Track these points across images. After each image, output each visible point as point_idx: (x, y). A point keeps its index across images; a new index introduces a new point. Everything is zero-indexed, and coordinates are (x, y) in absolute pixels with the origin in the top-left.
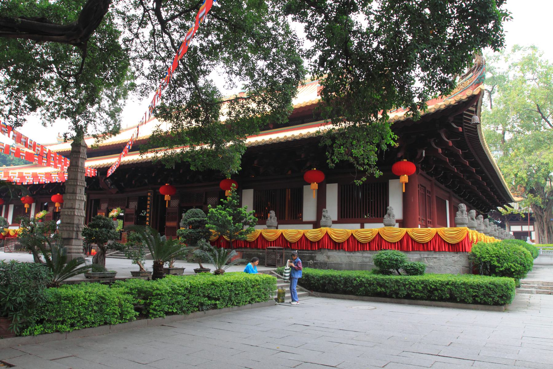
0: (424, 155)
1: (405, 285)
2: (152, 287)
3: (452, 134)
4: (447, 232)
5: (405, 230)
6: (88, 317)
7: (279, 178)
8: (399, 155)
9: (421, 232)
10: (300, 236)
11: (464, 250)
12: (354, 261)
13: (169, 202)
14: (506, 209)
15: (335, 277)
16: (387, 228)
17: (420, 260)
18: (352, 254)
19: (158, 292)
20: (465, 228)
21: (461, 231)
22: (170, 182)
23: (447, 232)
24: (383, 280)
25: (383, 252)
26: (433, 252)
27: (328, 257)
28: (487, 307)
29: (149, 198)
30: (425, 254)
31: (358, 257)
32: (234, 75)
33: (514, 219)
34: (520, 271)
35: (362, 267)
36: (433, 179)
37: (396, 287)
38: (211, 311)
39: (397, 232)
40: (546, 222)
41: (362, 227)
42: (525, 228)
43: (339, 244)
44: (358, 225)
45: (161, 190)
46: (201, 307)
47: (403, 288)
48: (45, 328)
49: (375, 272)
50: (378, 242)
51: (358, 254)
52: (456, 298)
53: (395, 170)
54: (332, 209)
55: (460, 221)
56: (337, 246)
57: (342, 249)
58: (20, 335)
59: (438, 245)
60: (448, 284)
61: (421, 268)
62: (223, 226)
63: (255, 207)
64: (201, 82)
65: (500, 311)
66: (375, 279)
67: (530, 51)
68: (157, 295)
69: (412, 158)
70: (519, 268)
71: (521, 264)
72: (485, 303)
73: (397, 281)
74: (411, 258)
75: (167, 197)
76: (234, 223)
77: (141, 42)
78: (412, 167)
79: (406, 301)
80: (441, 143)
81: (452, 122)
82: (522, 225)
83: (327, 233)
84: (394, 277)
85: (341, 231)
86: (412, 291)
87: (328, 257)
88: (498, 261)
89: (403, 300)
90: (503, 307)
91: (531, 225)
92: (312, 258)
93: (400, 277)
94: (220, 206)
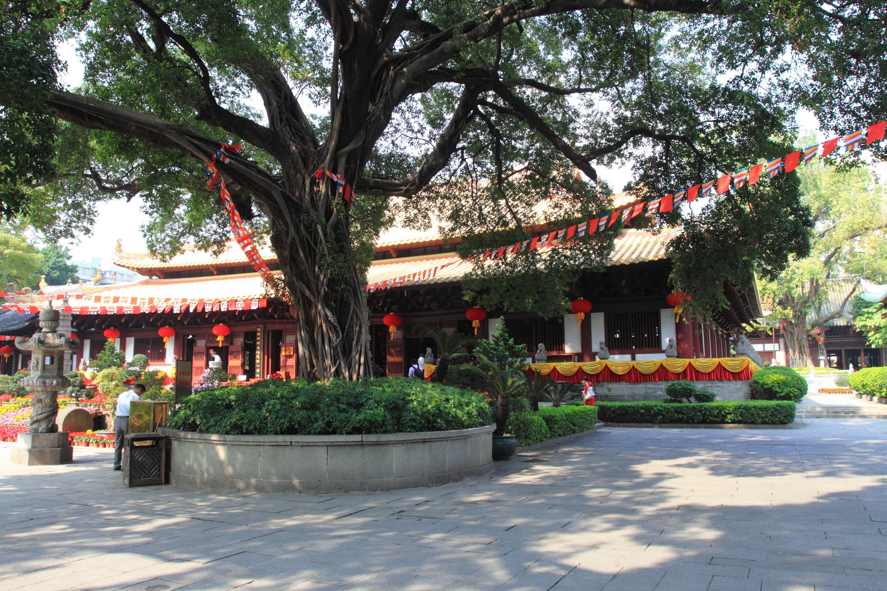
1: (701, 411)
10: (576, 369)
12: (637, 392)
14: (752, 326)
21: (744, 360)
23: (728, 363)
27: (609, 390)
28: (767, 426)
31: (641, 388)
40: (798, 340)
41: (633, 358)
42: (769, 347)
49: (666, 401)
50: (662, 373)
55: (741, 352)
59: (721, 374)
65: (784, 428)
66: (665, 408)
70: (797, 392)
72: (773, 423)
74: (699, 386)
79: (702, 425)
83: (606, 366)
85: (619, 361)
87: (609, 390)
90: (789, 424)
91: (776, 342)
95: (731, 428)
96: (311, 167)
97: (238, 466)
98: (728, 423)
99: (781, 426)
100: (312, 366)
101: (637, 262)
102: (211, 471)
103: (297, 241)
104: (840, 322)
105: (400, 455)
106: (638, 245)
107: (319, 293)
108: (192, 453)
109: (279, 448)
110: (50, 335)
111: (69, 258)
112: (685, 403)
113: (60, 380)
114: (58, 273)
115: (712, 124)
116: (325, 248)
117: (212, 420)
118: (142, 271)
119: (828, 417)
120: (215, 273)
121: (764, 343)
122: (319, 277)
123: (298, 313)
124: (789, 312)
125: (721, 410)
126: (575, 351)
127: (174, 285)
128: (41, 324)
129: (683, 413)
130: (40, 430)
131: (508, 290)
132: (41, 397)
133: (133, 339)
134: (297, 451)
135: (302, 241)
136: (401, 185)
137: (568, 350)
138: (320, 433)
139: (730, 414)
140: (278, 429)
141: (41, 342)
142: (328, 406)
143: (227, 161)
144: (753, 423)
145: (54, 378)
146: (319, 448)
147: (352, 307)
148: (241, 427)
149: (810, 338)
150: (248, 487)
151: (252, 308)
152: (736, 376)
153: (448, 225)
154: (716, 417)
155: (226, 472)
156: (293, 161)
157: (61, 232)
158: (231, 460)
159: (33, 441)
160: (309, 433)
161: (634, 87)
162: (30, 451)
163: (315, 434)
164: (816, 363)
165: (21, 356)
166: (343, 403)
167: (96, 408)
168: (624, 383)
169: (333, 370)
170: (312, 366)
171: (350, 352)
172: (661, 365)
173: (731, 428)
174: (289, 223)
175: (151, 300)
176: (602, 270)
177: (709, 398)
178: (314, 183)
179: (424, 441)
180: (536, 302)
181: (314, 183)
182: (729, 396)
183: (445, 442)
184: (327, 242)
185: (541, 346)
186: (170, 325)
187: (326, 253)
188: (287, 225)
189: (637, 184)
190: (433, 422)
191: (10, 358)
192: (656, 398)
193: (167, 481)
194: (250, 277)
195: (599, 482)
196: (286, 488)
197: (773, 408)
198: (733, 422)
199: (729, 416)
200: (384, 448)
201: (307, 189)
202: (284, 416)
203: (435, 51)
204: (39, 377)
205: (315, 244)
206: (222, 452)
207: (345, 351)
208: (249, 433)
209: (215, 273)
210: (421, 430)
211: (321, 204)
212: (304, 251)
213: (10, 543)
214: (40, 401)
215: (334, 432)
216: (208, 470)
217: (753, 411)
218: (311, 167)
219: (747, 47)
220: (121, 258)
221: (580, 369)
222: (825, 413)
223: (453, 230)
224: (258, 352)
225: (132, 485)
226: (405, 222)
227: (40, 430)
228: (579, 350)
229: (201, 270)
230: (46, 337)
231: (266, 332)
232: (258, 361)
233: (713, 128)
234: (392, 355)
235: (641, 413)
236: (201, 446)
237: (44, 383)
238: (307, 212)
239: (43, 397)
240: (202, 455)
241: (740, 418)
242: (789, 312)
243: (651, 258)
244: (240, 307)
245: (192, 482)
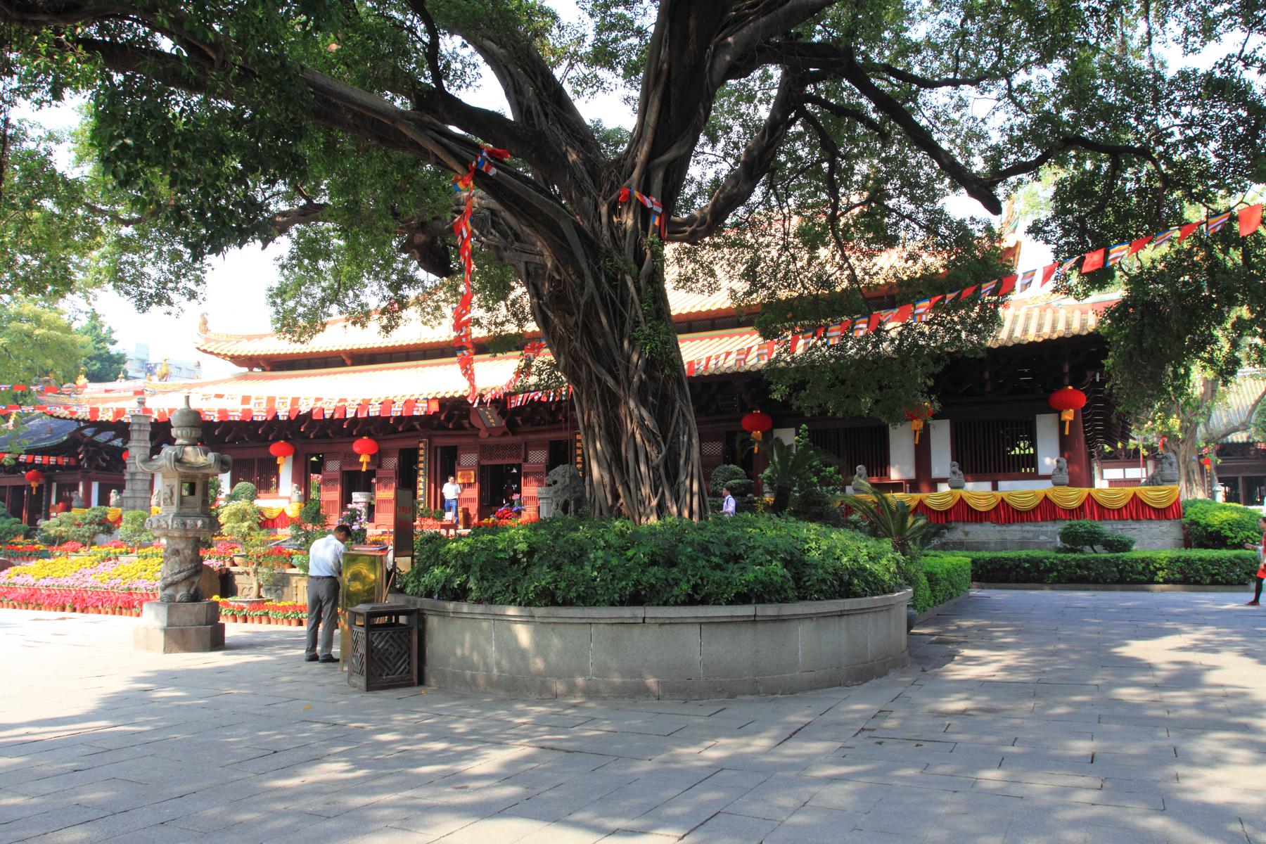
1: (1117, 566)
11: (1180, 516)
15: (1011, 559)
18: (1004, 528)
21: (1173, 490)
27: (966, 534)
31: (1014, 532)
41: (995, 488)
43: (1164, 509)
49: (1059, 550)
50: (1046, 510)
51: (1016, 527)
54: (942, 463)
55: (1169, 478)
60: (1178, 561)
66: (1062, 561)
74: (1108, 528)
79: (1118, 586)
82: (1124, 466)
83: (961, 499)
85: (978, 492)
87: (966, 534)
88: (1231, 530)
95: (1162, 591)
96: (607, 187)
97: (553, 657)
98: (1159, 583)
99: (1241, 587)
100: (616, 497)
101: (1010, 344)
102: (505, 664)
103: (598, 300)
104: (1239, 437)
105: (809, 637)
106: (1028, 318)
107: (630, 383)
108: (467, 637)
109: (622, 628)
110: (189, 449)
111: (114, 343)
112: (1088, 553)
113: (207, 520)
114: (98, 365)
115: (1176, 130)
116: (640, 312)
117: (498, 584)
118: (238, 360)
120: (348, 362)
121: (1124, 467)
122: (629, 359)
123: (588, 415)
125: (1148, 564)
126: (905, 477)
127: (287, 380)
128: (174, 432)
129: (1089, 569)
130: (178, 597)
131: (833, 385)
132: (177, 547)
134: (653, 632)
135: (603, 300)
137: (895, 475)
138: (684, 604)
139: (1162, 569)
140: (616, 596)
141: (179, 460)
142: (693, 559)
143: (493, 172)
144: (1197, 583)
145: (198, 516)
146: (689, 628)
147: (678, 405)
148: (553, 595)
150: (571, 690)
151: (415, 413)
152: (1160, 514)
153: (742, 286)
154: (1140, 573)
155: (531, 666)
156: (573, 176)
157: (151, 296)
158: (541, 648)
159: (170, 615)
160: (666, 604)
161: (1043, 77)
162: (166, 631)
163: (676, 604)
165: (55, 485)
166: (716, 556)
167: (221, 563)
168: (988, 523)
169: (654, 502)
170: (616, 497)
171: (676, 476)
172: (1046, 497)
173: (1162, 591)
174: (587, 271)
175: (295, 401)
176: (982, 355)
177: (1125, 546)
178: (613, 210)
179: (841, 614)
180: (877, 402)
181: (613, 210)
182: (1154, 542)
183: (866, 616)
184: (641, 302)
185: (860, 468)
186: (286, 439)
187: (642, 319)
188: (581, 276)
189: (1047, 224)
190: (846, 584)
191: (40, 488)
192: (1040, 546)
193: (421, 681)
194: (402, 368)
196: (637, 692)
197: (1230, 560)
198: (1166, 582)
199: (1160, 573)
200: (785, 625)
201: (604, 219)
202: (626, 577)
203: (781, 10)
204: (177, 515)
205: (623, 303)
206: (524, 635)
207: (669, 474)
208: (567, 603)
209: (348, 362)
210: (831, 596)
211: (627, 245)
212: (607, 315)
213: (282, 799)
214: (177, 552)
215: (704, 602)
216: (498, 664)
217: (1198, 565)
218: (607, 187)
219: (844, 89)
220: (207, 340)
223: (749, 293)
224: (421, 479)
225: (371, 687)
226: (679, 282)
227: (178, 597)
228: (912, 475)
229: (326, 359)
230: (184, 452)
231: (431, 449)
232: (420, 492)
233: (1178, 137)
236: (485, 625)
237: (184, 524)
238: (608, 254)
239: (181, 546)
240: (488, 639)
241: (1178, 576)
243: (1031, 337)
244: (396, 411)
245: (474, 682)
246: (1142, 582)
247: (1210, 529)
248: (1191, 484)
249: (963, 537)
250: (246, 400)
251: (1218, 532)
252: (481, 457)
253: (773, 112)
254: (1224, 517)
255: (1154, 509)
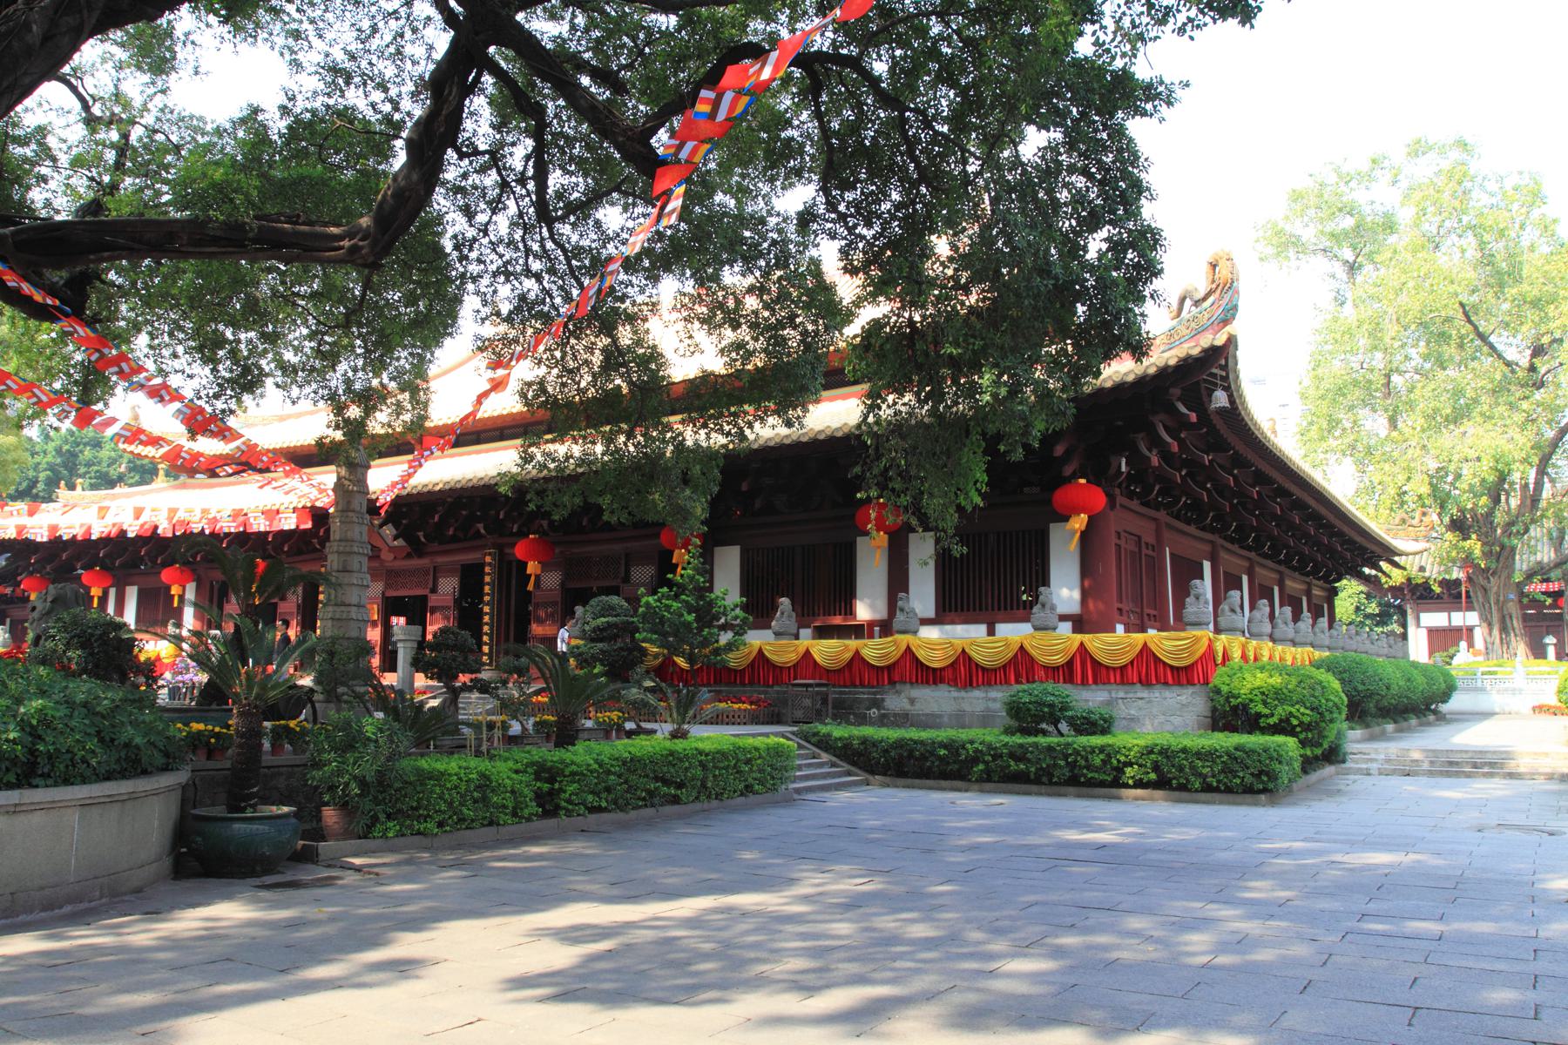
0: (1124, 469)
1: (1066, 757)
2: (562, 761)
3: (1178, 425)
4: (1166, 643)
5: (1079, 637)
6: (465, 811)
7: (796, 519)
8: (1068, 471)
9: (1116, 643)
10: (849, 655)
12: (968, 708)
13: (538, 577)
15: (922, 743)
16: (1038, 634)
17: (1109, 703)
18: (963, 694)
19: (574, 768)
20: (1207, 633)
21: (1197, 640)
22: (543, 533)
23: (1166, 643)
24: (1021, 746)
25: (1025, 687)
26: (1138, 686)
27: (912, 701)
28: (1230, 797)
29: (487, 569)
30: (1120, 692)
32: (697, 324)
33: (1420, 594)
34: (1310, 724)
35: (985, 720)
36: (1162, 515)
37: (1048, 761)
38: (669, 809)
39: (1060, 642)
41: (991, 632)
42: (1458, 619)
44: (983, 628)
45: (519, 551)
46: (650, 799)
47: (1062, 763)
48: (402, 825)
49: (1009, 731)
50: (1021, 665)
52: (1171, 780)
53: (1060, 505)
54: (922, 595)
55: (1192, 618)
56: (927, 675)
57: (1158, 682)
58: (365, 837)
61: (1105, 721)
62: (671, 633)
63: (747, 587)
64: (625, 336)
67: (1456, 155)
68: (573, 774)
69: (1100, 474)
71: (1312, 709)
72: (1229, 790)
73: (1050, 749)
74: (1089, 699)
75: (532, 567)
76: (700, 629)
77: (491, 242)
78: (1099, 499)
79: (1071, 789)
80: (1156, 442)
81: (1179, 399)
84: (1042, 740)
85: (935, 641)
86: (1081, 768)
87: (912, 701)
88: (1265, 703)
89: (1063, 789)
92: (878, 704)
93: (1062, 739)
94: (665, 589)
95: (1136, 799)
98: (1126, 786)
119: (1431, 773)
121: (1449, 610)
124: (1474, 545)
125: (1109, 756)
129: (1029, 760)
133: (135, 589)
136: (340, 238)
139: (1131, 764)
144: (1183, 788)
149: (1525, 600)
152: (1182, 676)
154: (1097, 770)
164: (1538, 652)
173: (1136, 799)
195: (848, 915)
197: (1228, 754)
198: (1139, 784)
221: (857, 653)
222: (1426, 766)
234: (540, 621)
235: (941, 758)
241: (1153, 776)
242: (1474, 545)
246: (1102, 784)
247: (1233, 702)
248: (1508, 634)
249: (908, 707)
250: (138, 513)
251: (1245, 707)
252: (388, 586)
253: (75, 48)
254: (1258, 683)
255: (1171, 667)
